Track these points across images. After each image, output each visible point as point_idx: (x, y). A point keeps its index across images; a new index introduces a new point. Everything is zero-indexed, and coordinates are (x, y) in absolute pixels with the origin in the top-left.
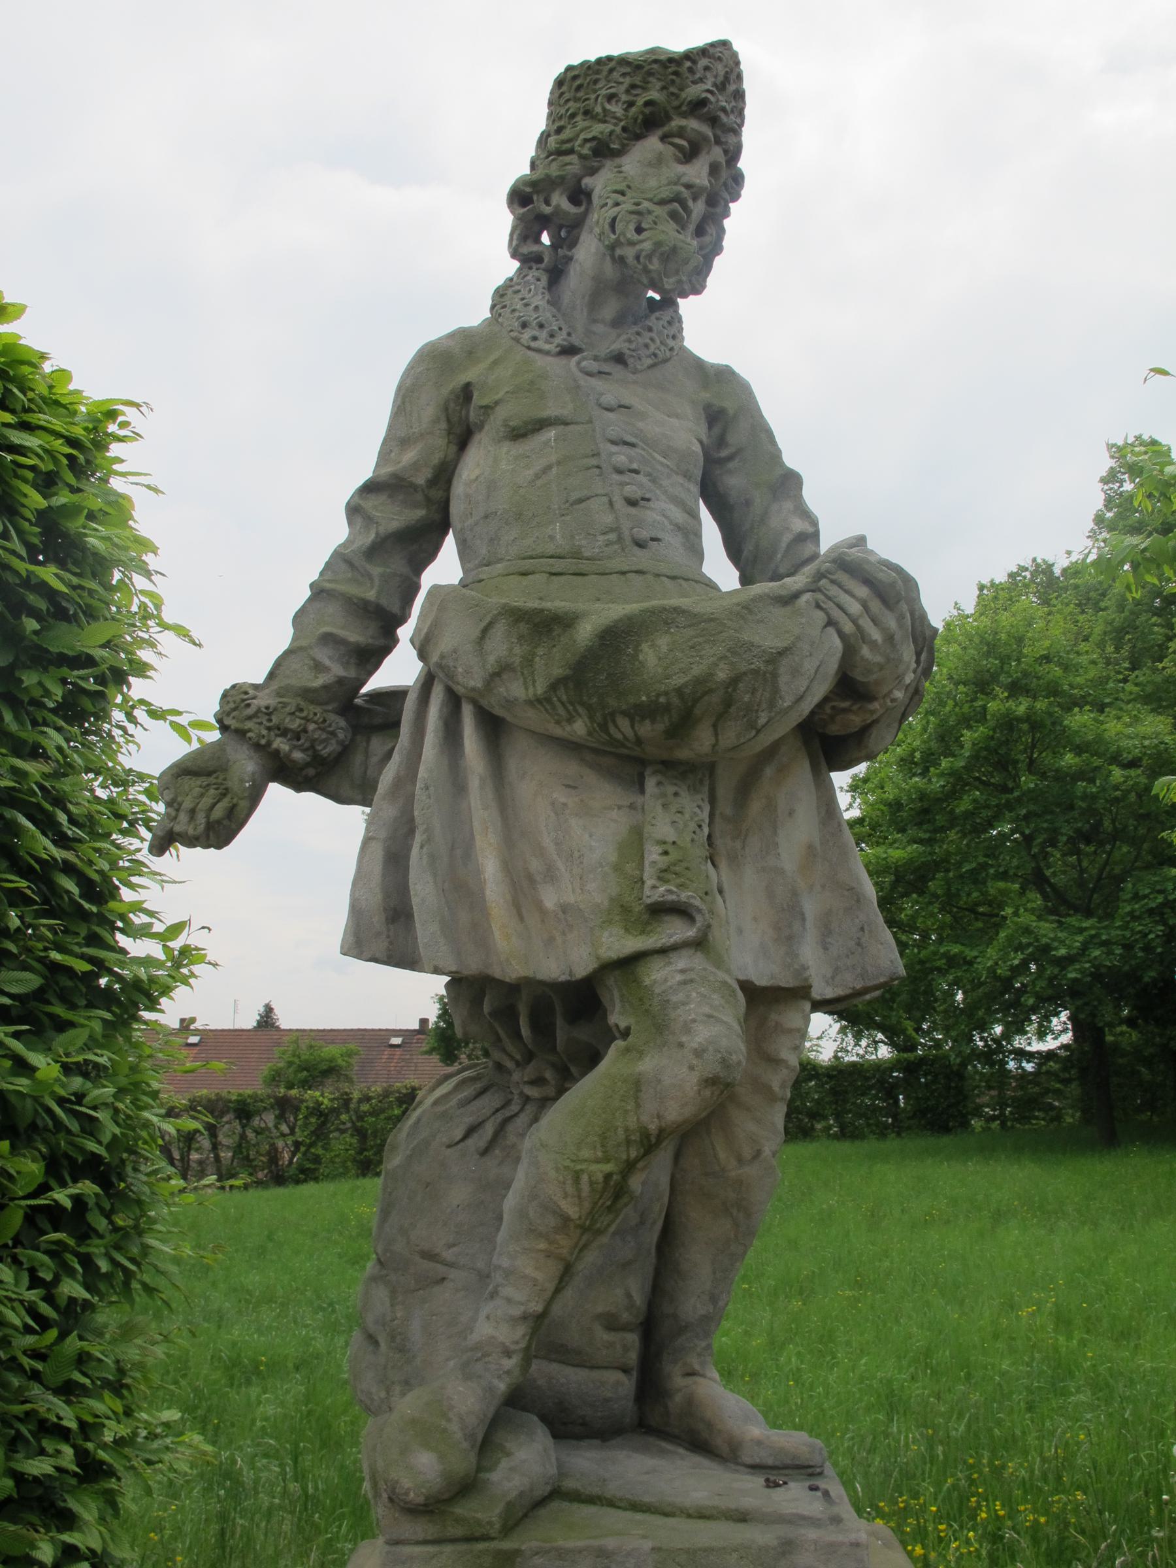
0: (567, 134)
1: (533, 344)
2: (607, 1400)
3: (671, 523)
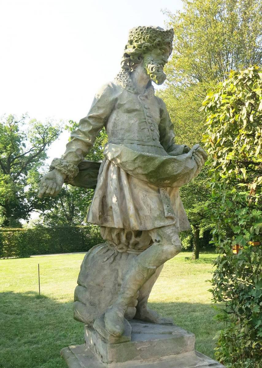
1: (129, 90)
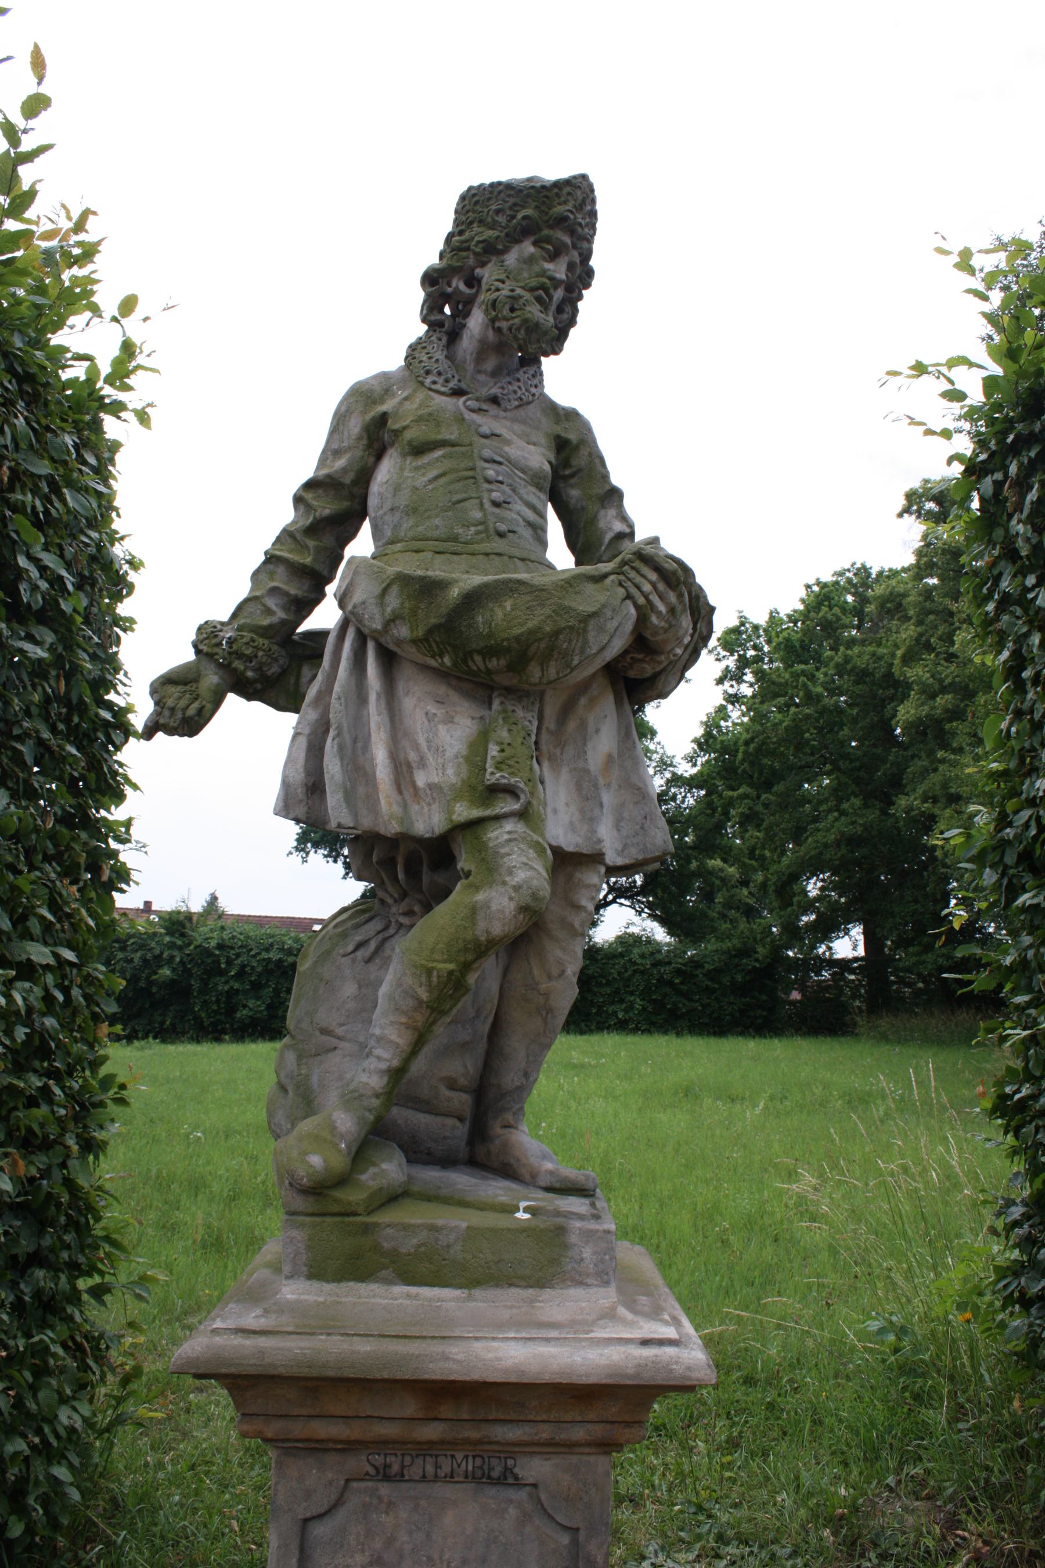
0: (467, 235)
2: (445, 1138)
3: (524, 520)
